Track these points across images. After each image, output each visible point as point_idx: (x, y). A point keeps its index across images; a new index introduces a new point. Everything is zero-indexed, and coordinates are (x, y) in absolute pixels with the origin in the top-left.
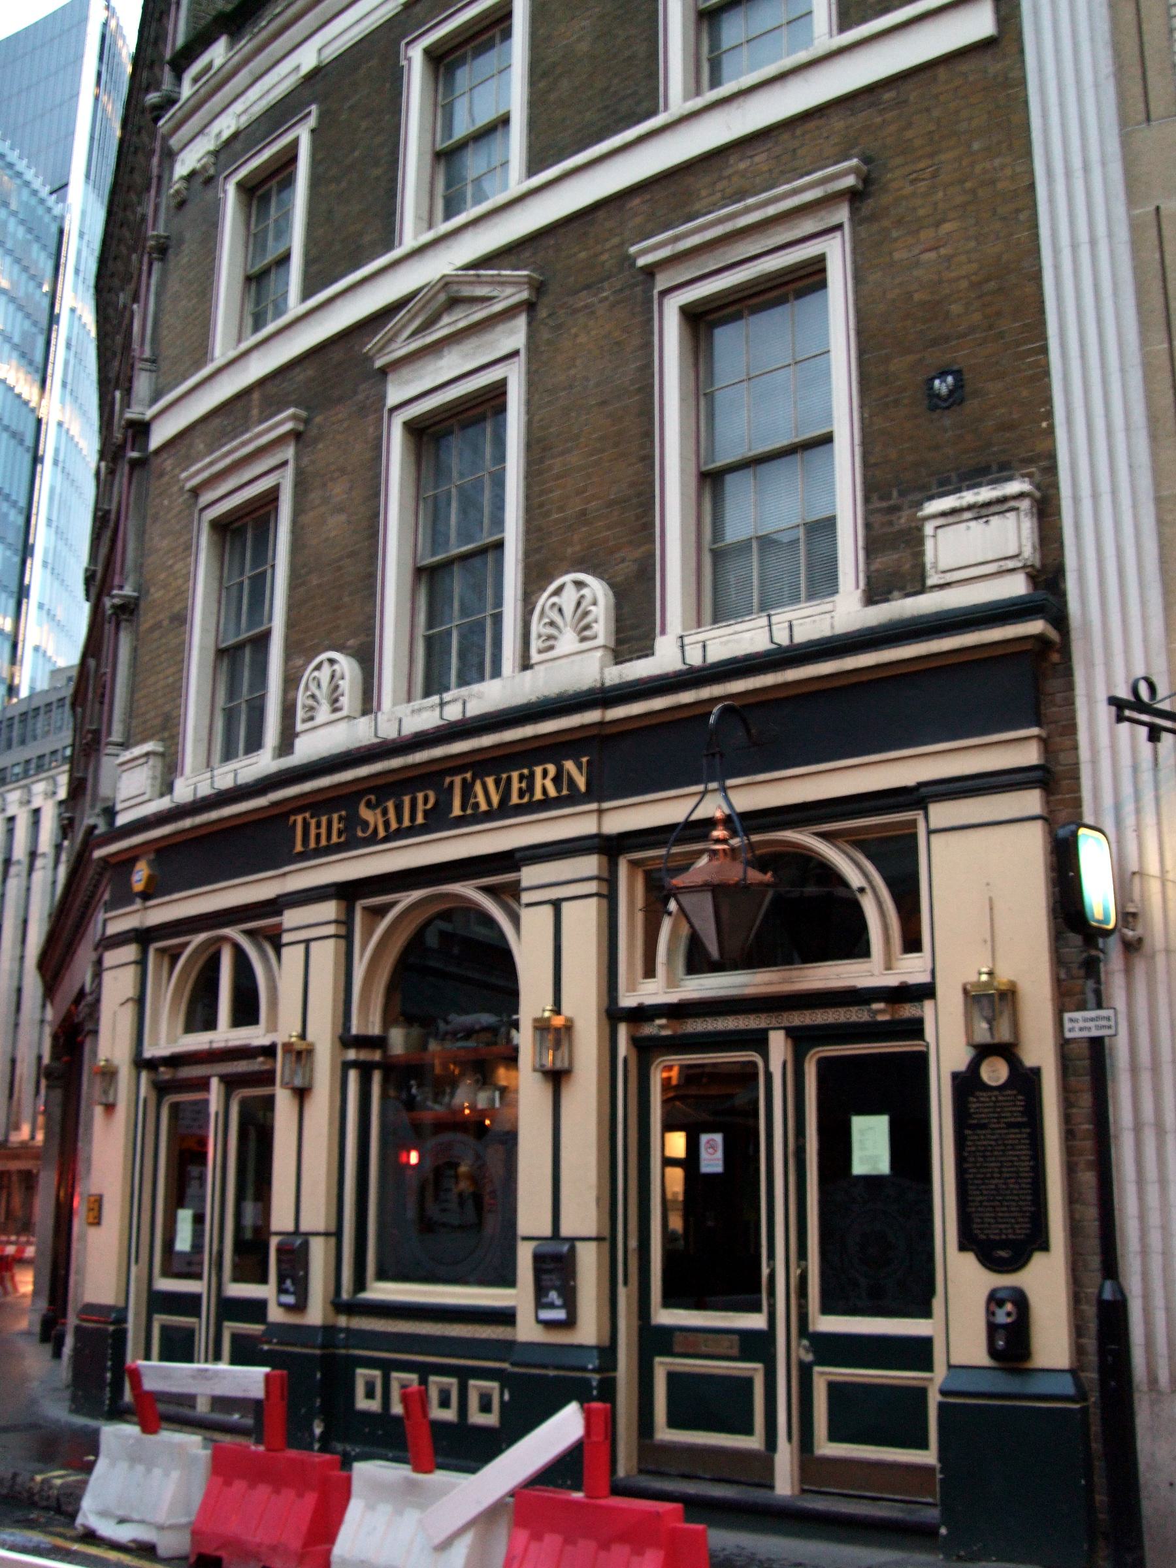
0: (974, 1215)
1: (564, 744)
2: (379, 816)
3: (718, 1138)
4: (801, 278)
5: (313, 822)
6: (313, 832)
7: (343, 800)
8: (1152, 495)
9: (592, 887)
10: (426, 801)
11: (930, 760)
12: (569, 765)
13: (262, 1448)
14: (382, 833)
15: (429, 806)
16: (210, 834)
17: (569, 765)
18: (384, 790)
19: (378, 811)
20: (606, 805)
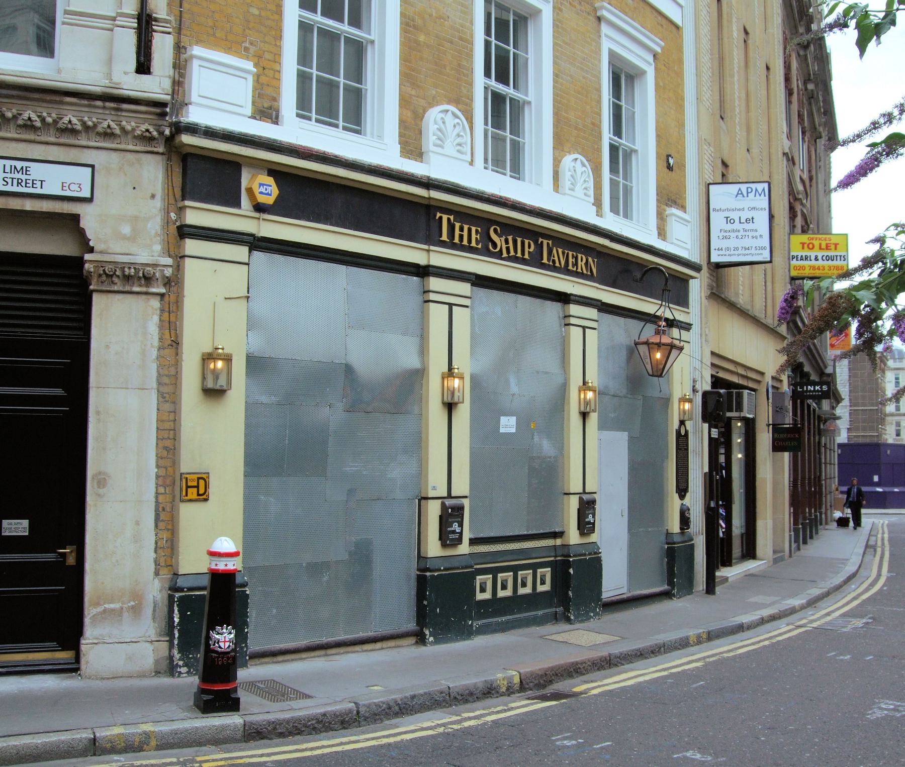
0: (888, 419)
1: (478, 217)
2: (503, 243)
3: (502, 418)
4: (637, 55)
5: (457, 225)
6: (457, 232)
7: (485, 222)
8: (172, 61)
9: (432, 297)
10: (529, 247)
11: (595, 290)
12: (590, 259)
13: (721, 535)
14: (505, 255)
15: (531, 250)
16: (609, 255)
17: (590, 259)
18: (509, 228)
19: (503, 239)
20: (432, 248)
